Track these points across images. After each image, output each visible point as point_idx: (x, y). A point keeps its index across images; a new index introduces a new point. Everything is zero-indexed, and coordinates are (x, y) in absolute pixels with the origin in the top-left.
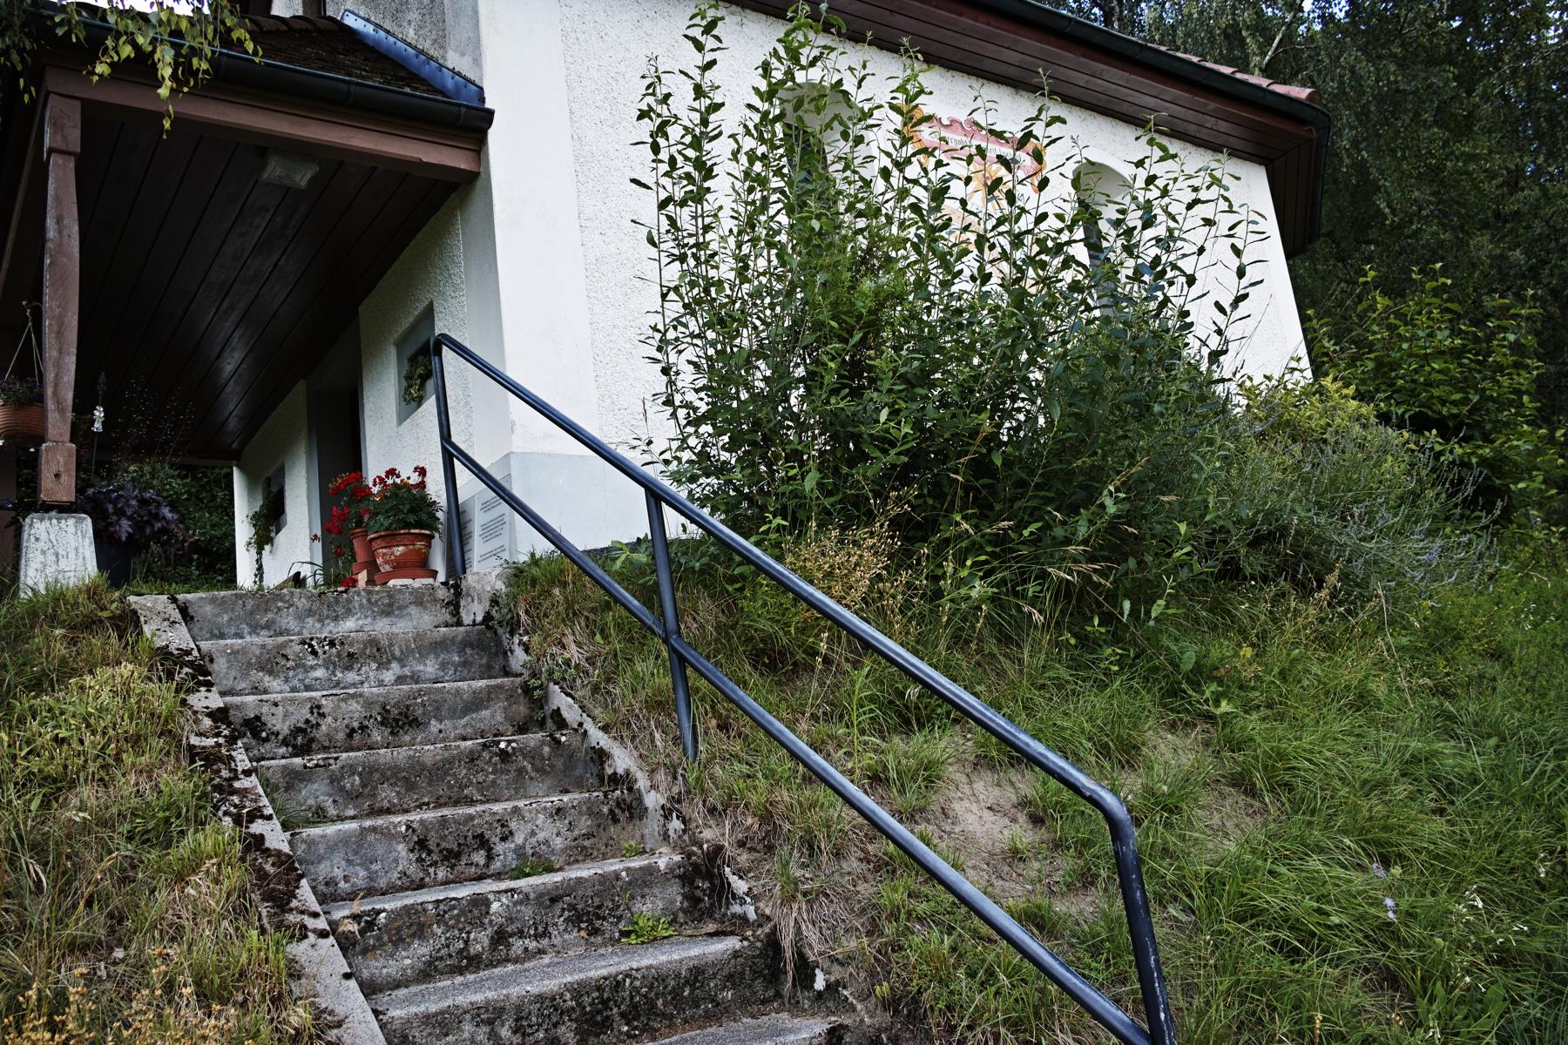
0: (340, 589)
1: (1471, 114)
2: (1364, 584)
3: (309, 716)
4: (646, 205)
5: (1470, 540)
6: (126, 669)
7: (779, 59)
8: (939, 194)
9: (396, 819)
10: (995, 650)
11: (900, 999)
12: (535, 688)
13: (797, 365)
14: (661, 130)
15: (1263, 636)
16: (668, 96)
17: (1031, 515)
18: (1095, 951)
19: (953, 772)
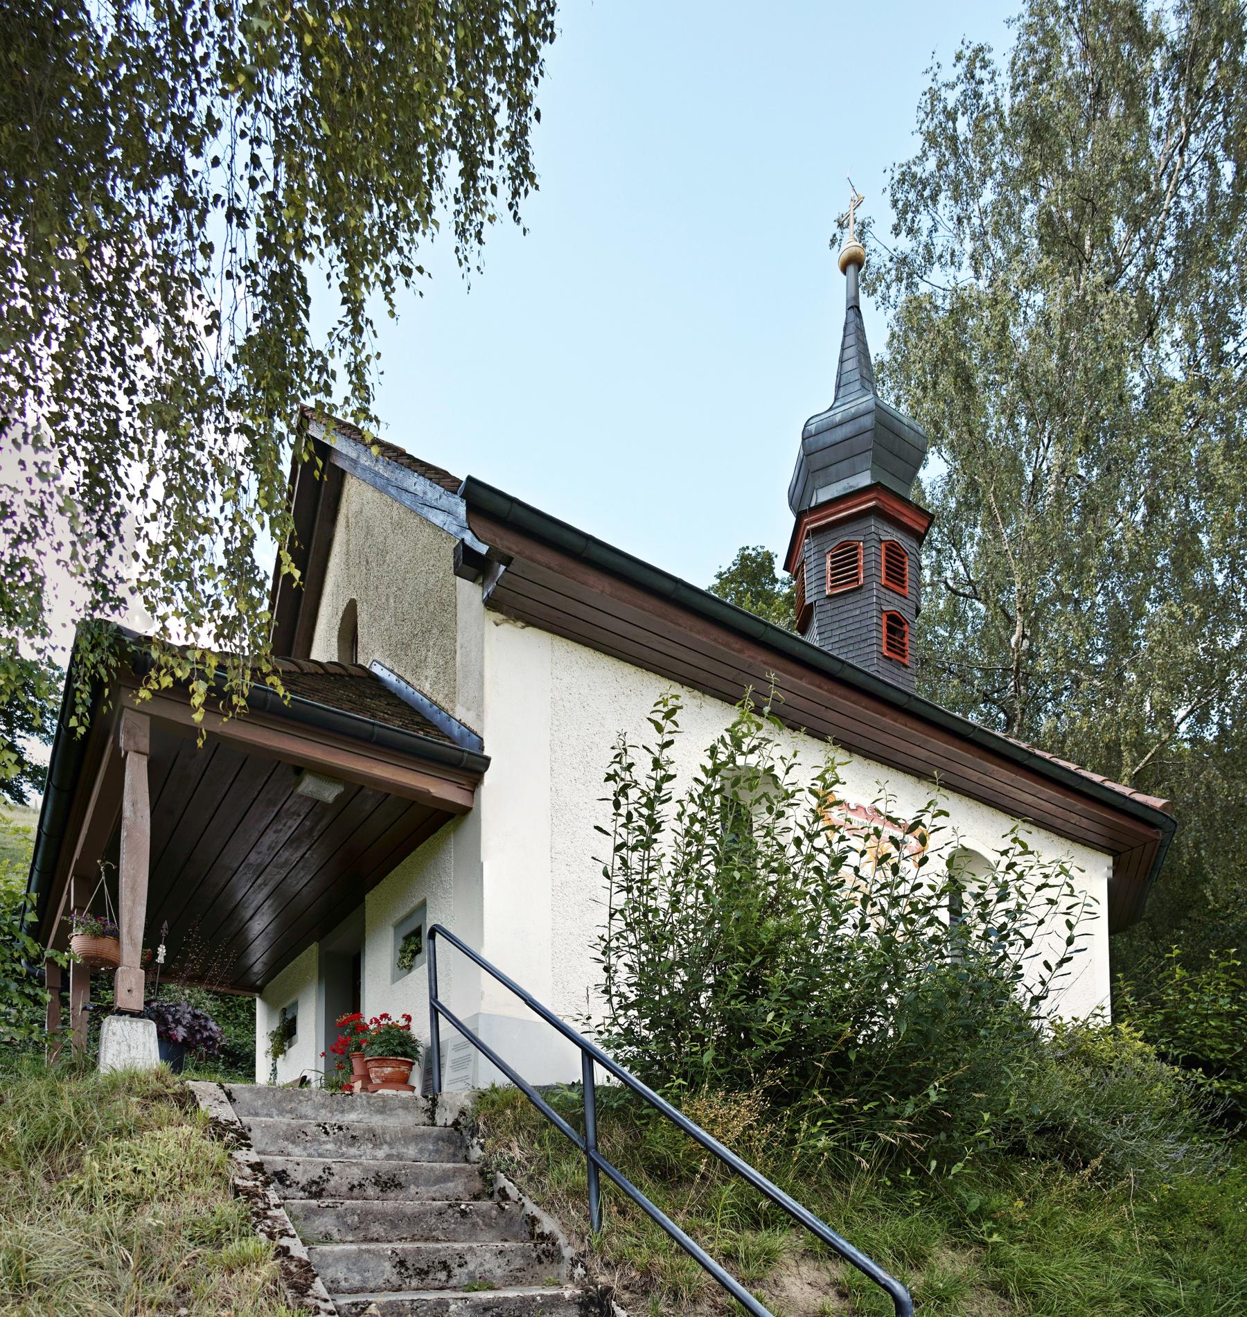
6: (186, 1129)
7: (725, 745)
8: (838, 862)
9: (386, 1246)
10: (830, 1183)
13: (709, 975)
14: (623, 791)
17: (872, 1096)
19: (786, 1258)
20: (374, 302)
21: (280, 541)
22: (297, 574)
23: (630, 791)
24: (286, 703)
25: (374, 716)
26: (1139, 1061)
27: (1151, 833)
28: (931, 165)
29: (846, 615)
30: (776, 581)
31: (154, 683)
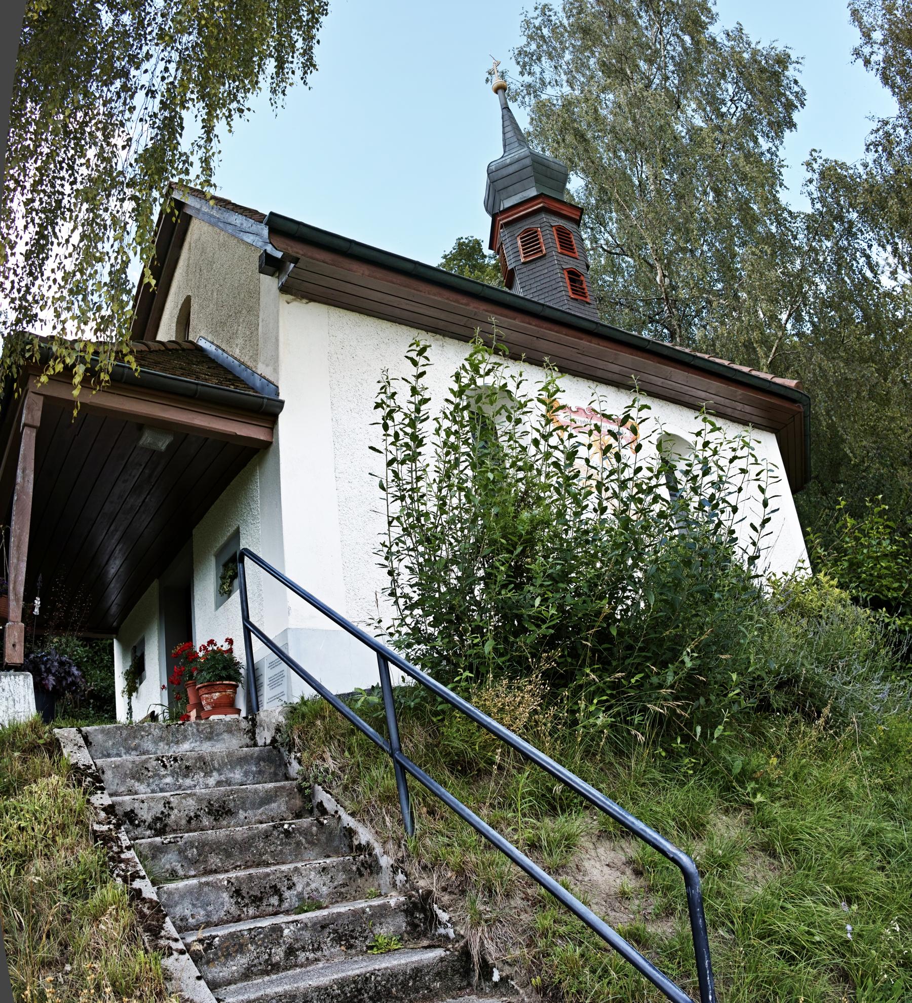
0: (180, 722)
1: (888, 393)
2: (845, 715)
3: (163, 809)
4: (379, 463)
5: (906, 684)
6: (54, 779)
7: (466, 371)
8: (571, 455)
9: (221, 876)
10: (613, 760)
11: (547, 987)
12: (306, 788)
13: (479, 569)
14: (390, 415)
15: (784, 750)
16: (394, 394)
17: (636, 668)
18: (672, 957)
19: (584, 841)
20: (220, 127)
21: (145, 262)
22: (153, 282)
23: (395, 415)
24: (136, 374)
25: (198, 378)
26: (840, 607)
27: (794, 407)
28: (533, 47)
29: (538, 274)
30: (485, 257)
31: (51, 369)
